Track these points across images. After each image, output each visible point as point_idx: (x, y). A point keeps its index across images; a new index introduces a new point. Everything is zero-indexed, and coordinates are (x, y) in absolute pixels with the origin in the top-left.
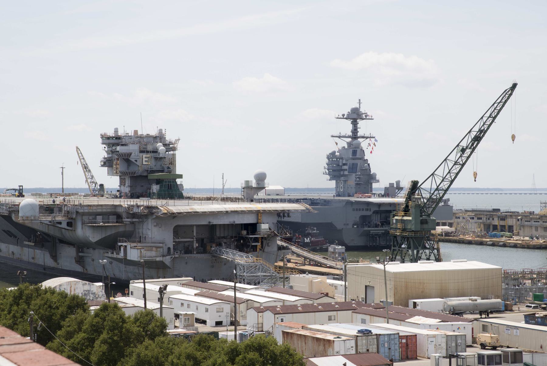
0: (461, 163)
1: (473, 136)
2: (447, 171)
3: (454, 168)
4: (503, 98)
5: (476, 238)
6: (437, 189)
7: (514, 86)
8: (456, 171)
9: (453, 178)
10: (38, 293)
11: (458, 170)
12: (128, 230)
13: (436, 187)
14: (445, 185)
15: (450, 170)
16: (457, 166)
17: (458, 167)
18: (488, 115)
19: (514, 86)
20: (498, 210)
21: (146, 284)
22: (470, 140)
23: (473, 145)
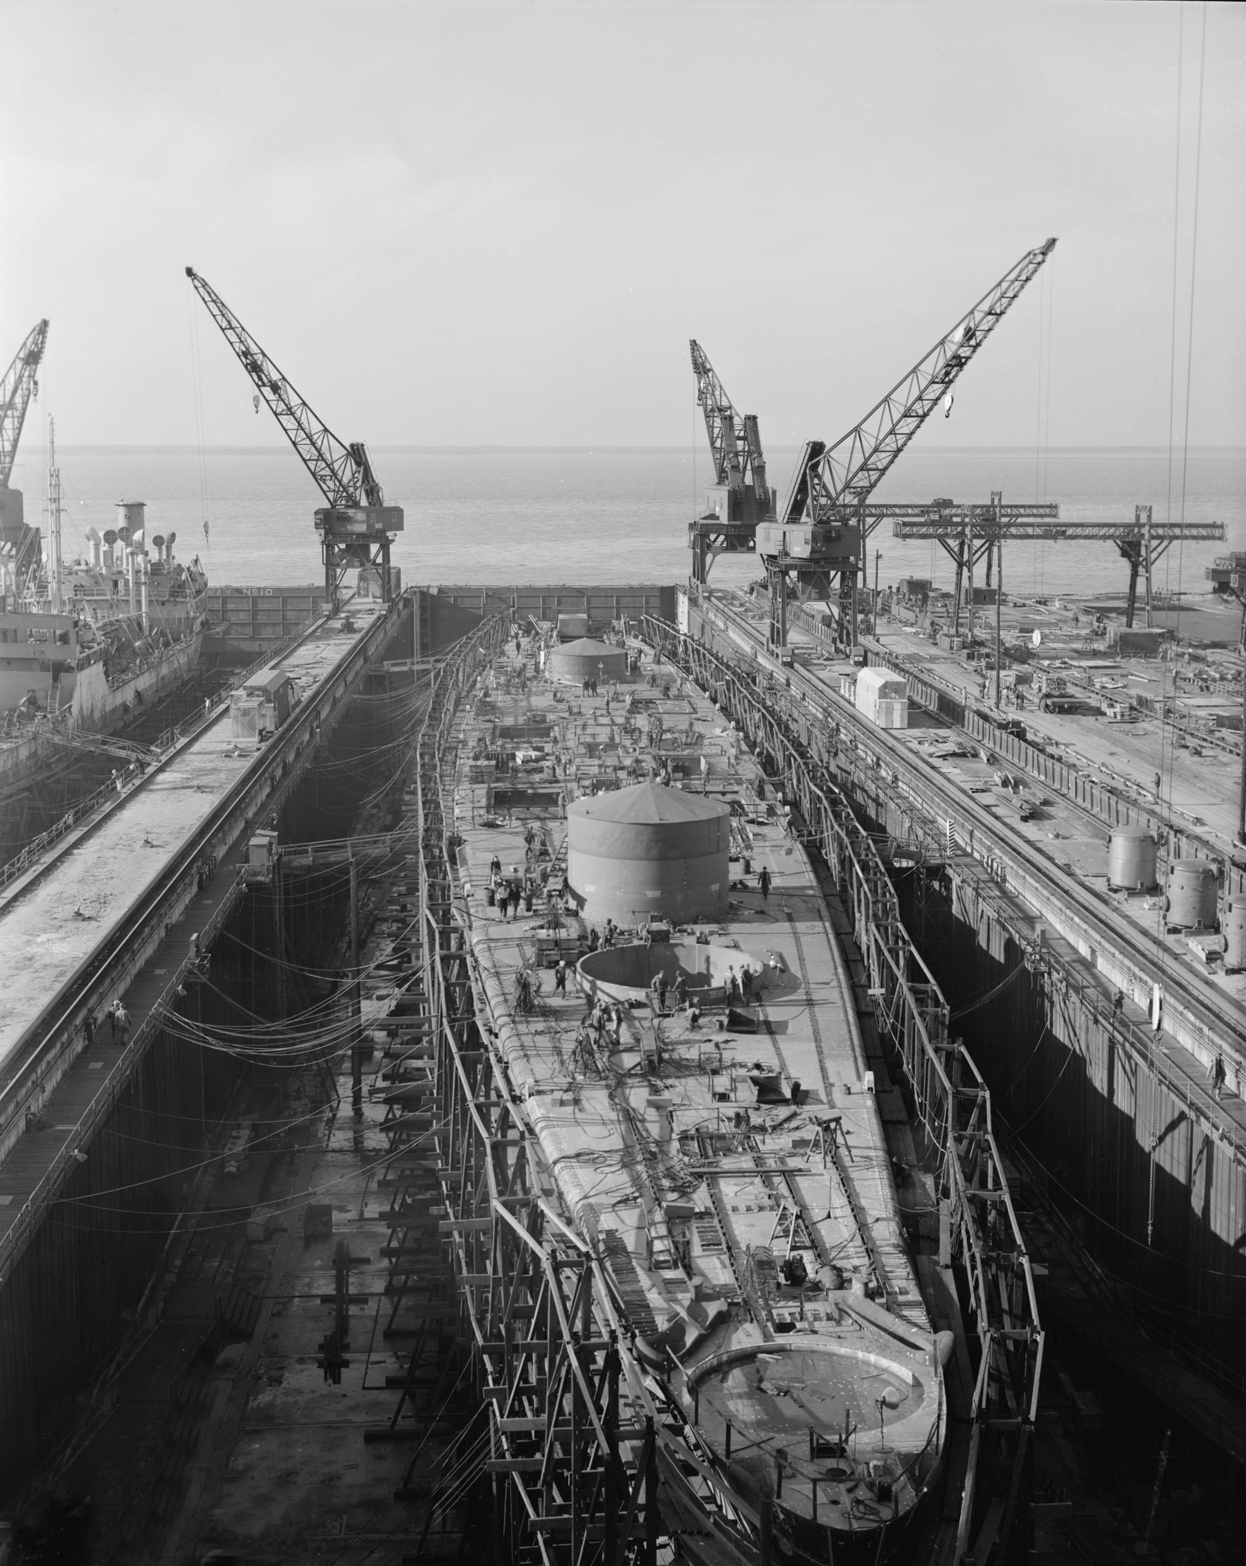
0: (921, 412)
1: (949, 354)
2: (887, 426)
3: (930, 389)
4: (1021, 271)
5: (418, 1069)
6: (863, 468)
7: (1052, 242)
8: (933, 396)
9: (900, 443)
10: (341, 1282)
11: (912, 426)
12: (812, 876)
13: (891, 426)
14: (881, 460)
15: (894, 426)
16: (909, 420)
17: (912, 422)
18: (985, 307)
19: (1052, 242)
20: (947, 504)
21: (1126, 589)
22: (941, 363)
23: (947, 374)
